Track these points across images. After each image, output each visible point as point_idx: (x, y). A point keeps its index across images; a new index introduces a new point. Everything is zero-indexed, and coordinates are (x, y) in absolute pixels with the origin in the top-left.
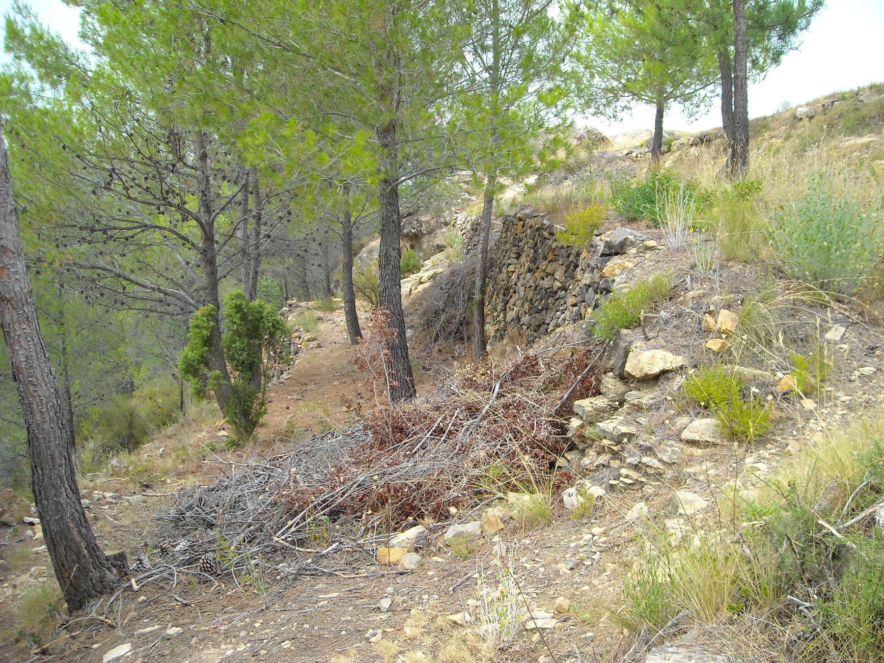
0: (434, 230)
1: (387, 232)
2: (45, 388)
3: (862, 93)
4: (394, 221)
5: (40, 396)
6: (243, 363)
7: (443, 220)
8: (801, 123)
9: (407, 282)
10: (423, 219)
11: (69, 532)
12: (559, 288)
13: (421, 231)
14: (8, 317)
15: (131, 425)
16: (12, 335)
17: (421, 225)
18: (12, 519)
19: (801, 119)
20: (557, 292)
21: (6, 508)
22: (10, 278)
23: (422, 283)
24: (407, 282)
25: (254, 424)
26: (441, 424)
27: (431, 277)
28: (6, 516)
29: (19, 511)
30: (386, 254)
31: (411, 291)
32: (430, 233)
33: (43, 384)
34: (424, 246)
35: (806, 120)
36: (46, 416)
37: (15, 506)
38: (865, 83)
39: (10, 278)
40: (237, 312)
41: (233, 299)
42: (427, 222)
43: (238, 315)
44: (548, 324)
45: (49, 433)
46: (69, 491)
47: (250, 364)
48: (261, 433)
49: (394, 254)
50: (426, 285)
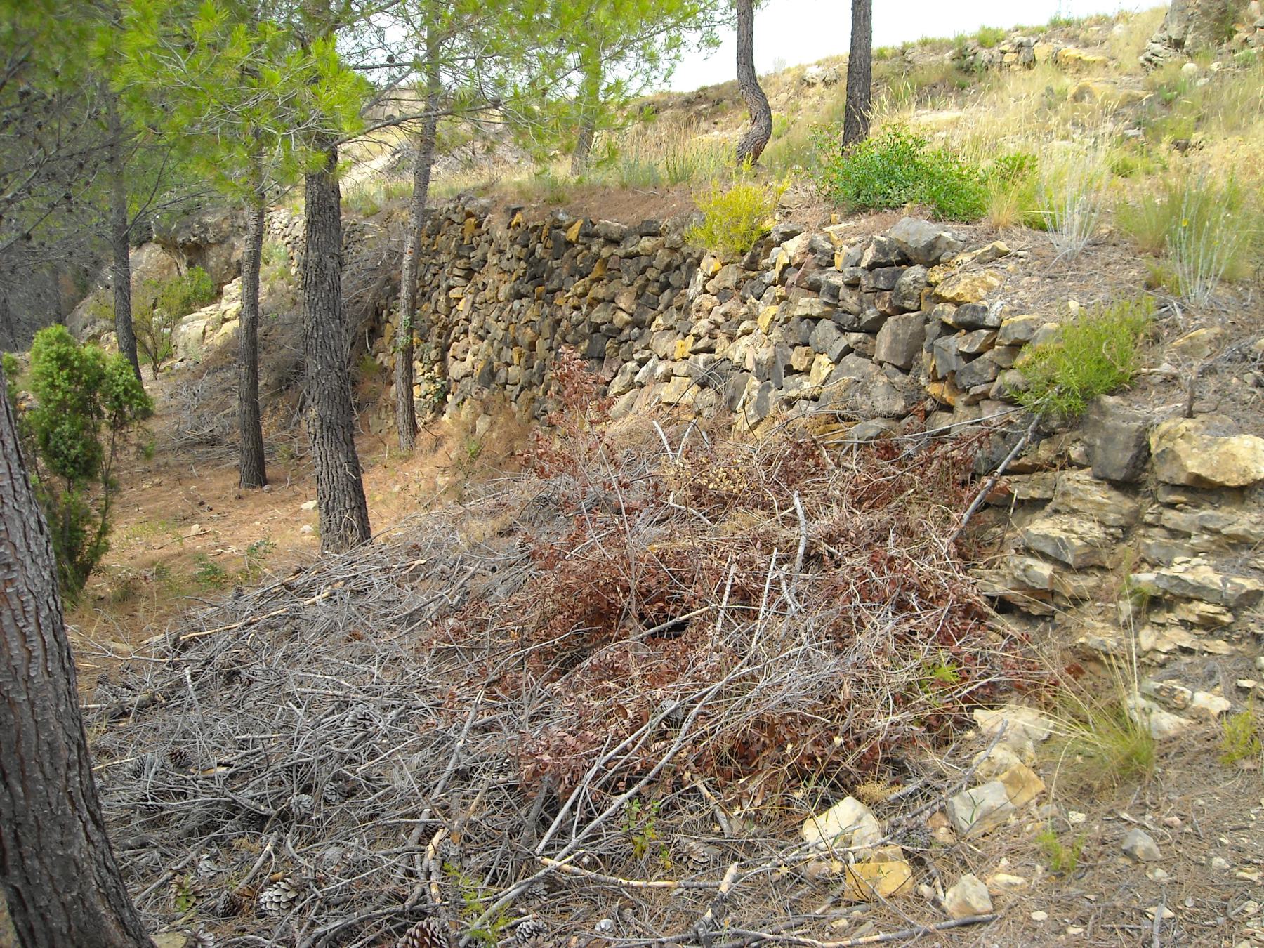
1: (320, 225)
2: (32, 571)
3: (909, 50)
4: (331, 208)
5: (19, 594)
6: (75, 461)
8: (812, 90)
9: (198, 318)
10: (208, 220)
11: (100, 928)
12: (627, 323)
13: (205, 238)
17: (206, 230)
19: (814, 84)
20: (621, 330)
23: (227, 320)
24: (198, 318)
25: (84, 571)
26: (737, 580)
30: (318, 264)
31: (204, 332)
32: (220, 243)
33: (28, 562)
34: (211, 263)
35: (820, 86)
36: (36, 644)
38: (913, 38)
40: (61, 368)
41: (51, 344)
42: (217, 225)
43: (65, 373)
44: (608, 383)
45: (42, 689)
46: (91, 826)
47: (87, 462)
48: (98, 585)
50: (236, 323)
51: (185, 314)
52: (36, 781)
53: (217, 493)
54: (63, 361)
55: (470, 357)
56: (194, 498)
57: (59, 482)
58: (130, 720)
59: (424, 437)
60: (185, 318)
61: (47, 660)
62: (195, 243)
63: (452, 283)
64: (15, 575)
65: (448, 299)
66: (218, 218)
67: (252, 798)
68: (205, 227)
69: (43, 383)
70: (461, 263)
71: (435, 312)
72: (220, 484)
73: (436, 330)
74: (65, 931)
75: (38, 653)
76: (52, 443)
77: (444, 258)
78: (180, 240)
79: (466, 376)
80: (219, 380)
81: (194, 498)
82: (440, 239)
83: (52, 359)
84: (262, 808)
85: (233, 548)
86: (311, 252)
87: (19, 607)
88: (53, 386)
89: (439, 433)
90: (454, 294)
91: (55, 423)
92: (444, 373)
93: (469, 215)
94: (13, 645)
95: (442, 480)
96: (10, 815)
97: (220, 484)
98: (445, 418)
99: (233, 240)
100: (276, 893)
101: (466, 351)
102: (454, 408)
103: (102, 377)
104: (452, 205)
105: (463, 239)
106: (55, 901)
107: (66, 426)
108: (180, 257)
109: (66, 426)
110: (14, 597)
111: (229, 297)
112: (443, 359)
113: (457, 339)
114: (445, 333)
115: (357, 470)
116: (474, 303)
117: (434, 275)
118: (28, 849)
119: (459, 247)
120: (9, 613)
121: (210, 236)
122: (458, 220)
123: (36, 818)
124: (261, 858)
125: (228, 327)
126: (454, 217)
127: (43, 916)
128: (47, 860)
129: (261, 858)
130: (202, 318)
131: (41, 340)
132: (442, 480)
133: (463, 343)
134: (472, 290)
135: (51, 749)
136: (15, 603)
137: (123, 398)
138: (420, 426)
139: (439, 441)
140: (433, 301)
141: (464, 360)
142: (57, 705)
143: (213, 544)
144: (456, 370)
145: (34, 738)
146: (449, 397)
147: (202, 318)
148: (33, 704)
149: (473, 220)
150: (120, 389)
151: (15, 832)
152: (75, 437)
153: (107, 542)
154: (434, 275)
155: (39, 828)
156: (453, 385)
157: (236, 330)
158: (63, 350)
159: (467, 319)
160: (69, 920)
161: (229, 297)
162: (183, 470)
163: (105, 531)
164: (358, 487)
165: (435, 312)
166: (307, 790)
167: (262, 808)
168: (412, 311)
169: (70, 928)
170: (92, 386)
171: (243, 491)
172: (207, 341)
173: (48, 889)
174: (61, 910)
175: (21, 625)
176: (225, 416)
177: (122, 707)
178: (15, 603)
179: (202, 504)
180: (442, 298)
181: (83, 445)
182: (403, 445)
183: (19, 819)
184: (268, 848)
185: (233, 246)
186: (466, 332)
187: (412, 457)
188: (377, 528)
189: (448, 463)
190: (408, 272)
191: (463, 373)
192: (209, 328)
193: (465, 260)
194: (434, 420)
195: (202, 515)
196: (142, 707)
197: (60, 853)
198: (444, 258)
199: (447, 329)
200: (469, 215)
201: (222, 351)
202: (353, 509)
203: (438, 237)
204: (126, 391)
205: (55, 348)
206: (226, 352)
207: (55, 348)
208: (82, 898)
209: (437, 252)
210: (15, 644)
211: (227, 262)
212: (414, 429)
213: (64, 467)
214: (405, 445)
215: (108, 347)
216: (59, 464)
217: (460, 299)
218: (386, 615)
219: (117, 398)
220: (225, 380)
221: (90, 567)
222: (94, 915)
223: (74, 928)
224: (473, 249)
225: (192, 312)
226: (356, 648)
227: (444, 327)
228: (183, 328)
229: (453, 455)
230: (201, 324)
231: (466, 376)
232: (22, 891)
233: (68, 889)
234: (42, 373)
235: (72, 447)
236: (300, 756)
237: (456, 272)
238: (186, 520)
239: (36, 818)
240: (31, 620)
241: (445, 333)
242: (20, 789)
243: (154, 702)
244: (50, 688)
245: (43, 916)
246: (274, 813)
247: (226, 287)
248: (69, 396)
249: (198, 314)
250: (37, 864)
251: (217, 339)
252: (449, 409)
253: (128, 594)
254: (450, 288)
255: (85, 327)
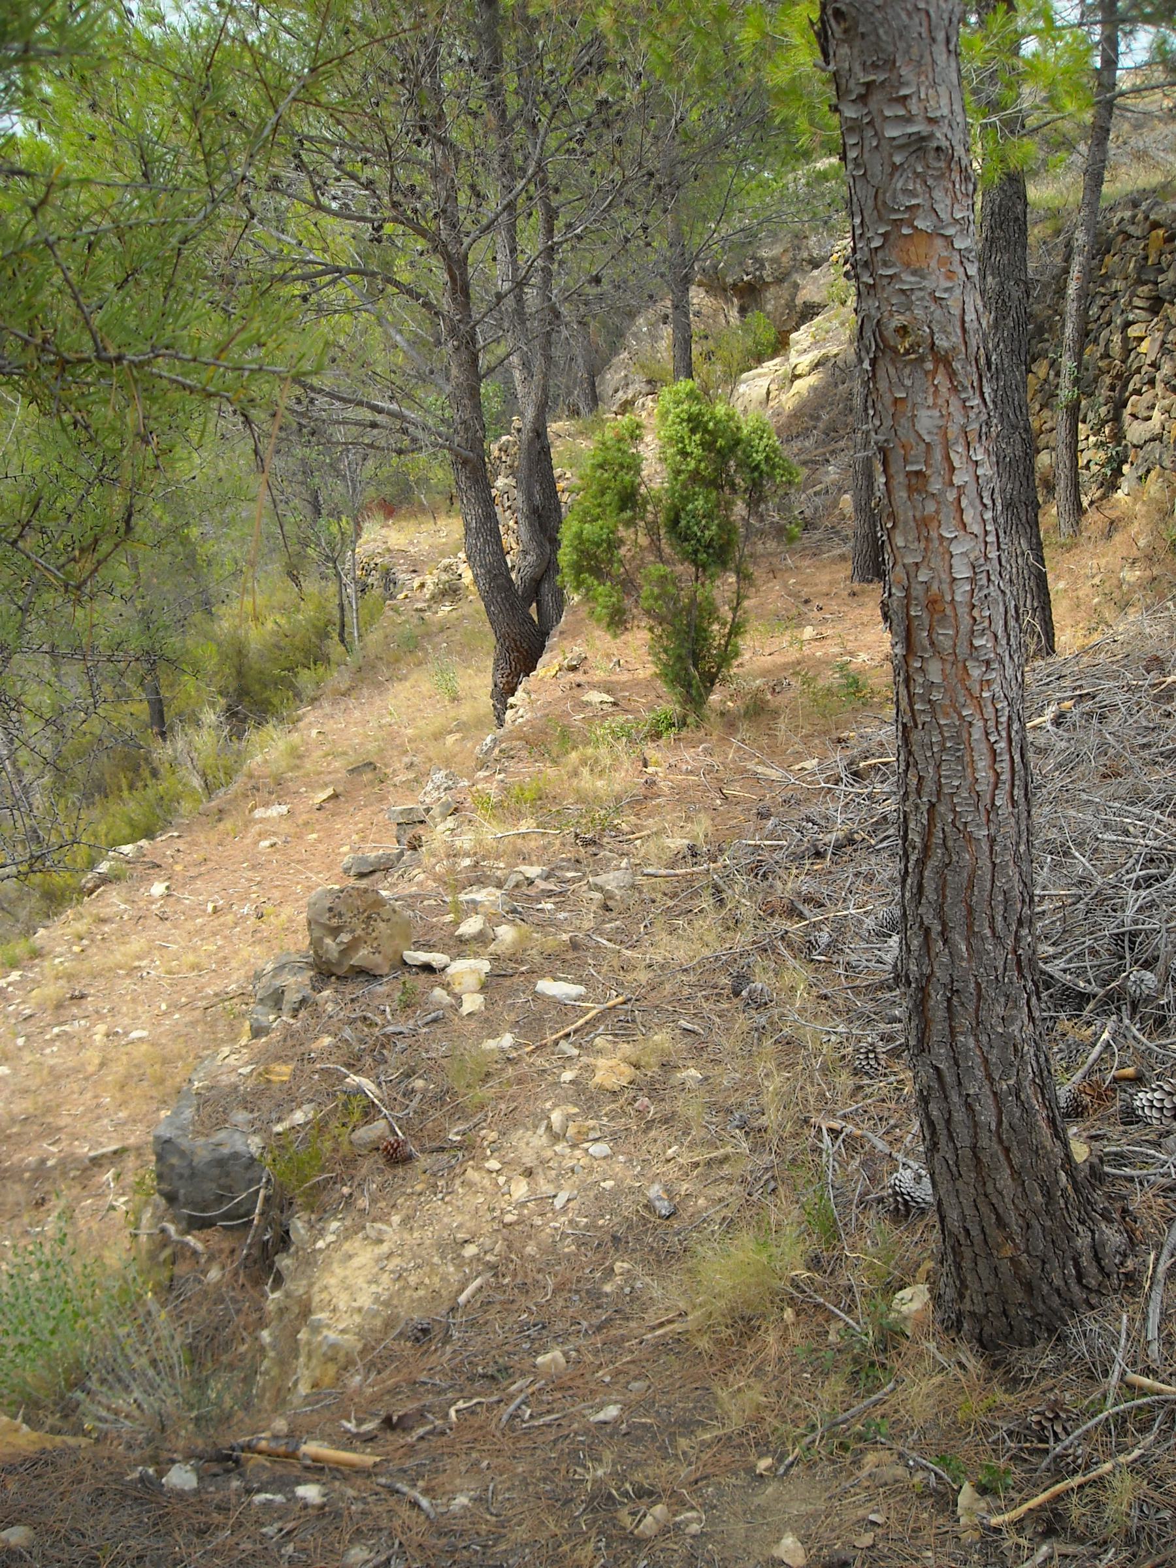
0: (788, 274)
1: (1003, 243)
4: (1017, 219)
6: (709, 546)
7: (805, 255)
9: (760, 376)
10: (764, 253)
11: (1032, 1127)
13: (761, 277)
14: (926, 421)
15: (240, 674)
16: (935, 486)
17: (762, 267)
18: (378, 958)
21: (359, 932)
22: (950, 275)
23: (799, 376)
24: (760, 376)
27: (817, 365)
28: (363, 952)
29: (391, 936)
32: (779, 281)
37: (382, 925)
39: (950, 275)
40: (693, 431)
42: (775, 260)
43: (697, 437)
49: (1017, 293)
50: (812, 380)
51: (742, 371)
52: (983, 939)
53: (824, 589)
54: (695, 423)
55: (1156, 413)
56: (796, 595)
57: (685, 570)
58: (828, 862)
59: (1093, 518)
60: (744, 376)
61: (1013, 785)
62: (749, 283)
63: (1131, 317)
64: (994, 675)
65: (1125, 339)
66: (777, 250)
67: (1065, 971)
68: (760, 262)
69: (671, 451)
70: (1144, 290)
71: (1106, 355)
72: (826, 578)
73: (1108, 380)
74: (993, 1127)
75: (1005, 777)
76: (683, 523)
77: (1117, 285)
78: (730, 280)
79: (1153, 440)
80: (796, 450)
81: (796, 595)
82: (1111, 261)
83: (683, 420)
84: (1082, 984)
85: (863, 656)
86: (989, 279)
87: (993, 716)
88: (684, 454)
89: (1114, 514)
90: (1133, 332)
91: (686, 499)
92: (1118, 436)
93: (1156, 225)
94: (981, 765)
95: (1131, 575)
96: (947, 980)
97: (826, 578)
98: (1120, 494)
99: (797, 278)
100: (1157, 1095)
101: (1152, 407)
102: (1134, 482)
103: (738, 442)
104: (1128, 214)
105: (1146, 258)
106: (986, 1090)
107: (700, 502)
108: (728, 301)
109: (700, 502)
110: (989, 704)
111: (798, 347)
112: (1117, 418)
113: (1138, 392)
114: (1119, 383)
115: (1041, 559)
116: (1164, 343)
117: (1103, 308)
118: (964, 1022)
119: (1141, 268)
120: (981, 723)
121: (767, 274)
122: (1139, 233)
123: (978, 985)
124: (1098, 1048)
125: (801, 385)
126: (1131, 229)
127: (969, 1107)
128: (984, 1039)
129: (1098, 1048)
130: (765, 375)
131: (668, 397)
132: (1131, 575)
133: (1148, 397)
134: (1161, 326)
135: (1006, 900)
136: (989, 712)
137: (763, 467)
138: (1085, 504)
139: (1113, 526)
140: (1102, 343)
141: (1149, 418)
142: (1018, 844)
143: (836, 650)
144: (1135, 432)
145: (988, 885)
146: (1126, 468)
147: (765, 375)
148: (992, 840)
149: (1161, 232)
150: (759, 457)
151: (949, 1000)
152: (708, 516)
153: (736, 646)
154: (1103, 308)
155: (980, 997)
156: (1132, 452)
157: (814, 389)
158: (695, 409)
159: (1152, 365)
160: (1000, 1113)
161: (798, 347)
162: (774, 560)
163: (736, 630)
164: (1041, 579)
165: (1106, 355)
166: (1147, 965)
167: (1082, 984)
168: (1079, 356)
169: (1000, 1123)
170: (723, 455)
171: (856, 586)
172: (771, 404)
173: (980, 1073)
174: (990, 1101)
175: (993, 739)
176: (816, 494)
177: (815, 846)
178: (989, 712)
179: (807, 602)
180: (1117, 338)
181: (719, 526)
182: (1064, 529)
183: (956, 985)
184: (1106, 1036)
185: (796, 286)
186: (1152, 382)
187: (1076, 545)
188: (1067, 638)
189: (1135, 553)
190: (1075, 304)
191: (1148, 436)
192: (773, 387)
193: (1150, 286)
194: (1104, 497)
195: (811, 615)
196: (838, 847)
197: (1000, 1030)
198: (1117, 285)
199: (1123, 379)
200: (1156, 225)
201: (797, 414)
202: (1034, 610)
203: (1107, 258)
204: (767, 458)
205: (685, 407)
206: (803, 415)
207: (685, 407)
208: (1017, 1092)
209: (1107, 277)
210: (982, 764)
211: (790, 305)
212: (1079, 510)
213: (696, 552)
214: (1066, 529)
215: (644, 414)
216: (690, 549)
217: (1142, 339)
218: (1144, 746)
219: (757, 467)
220: (801, 451)
221: (716, 675)
222: (1026, 1110)
223: (1005, 1125)
224: (1162, 271)
225: (750, 369)
226: (1120, 786)
227: (1118, 376)
228: (742, 388)
229: (1142, 543)
230: (764, 383)
231: (1153, 440)
232: (946, 1073)
233: (1005, 1076)
234: (670, 438)
235: (706, 527)
236: (1135, 922)
237: (1137, 302)
238: (799, 621)
239: (978, 985)
240: (1004, 734)
241: (1119, 383)
242: (964, 948)
243: (851, 841)
244: (1012, 821)
245: (969, 1107)
246: (1102, 992)
247: (794, 336)
248: (703, 465)
249: (759, 370)
250: (971, 1042)
251: (788, 400)
252: (1125, 486)
253: (758, 711)
254: (1128, 324)
255: (616, 391)
